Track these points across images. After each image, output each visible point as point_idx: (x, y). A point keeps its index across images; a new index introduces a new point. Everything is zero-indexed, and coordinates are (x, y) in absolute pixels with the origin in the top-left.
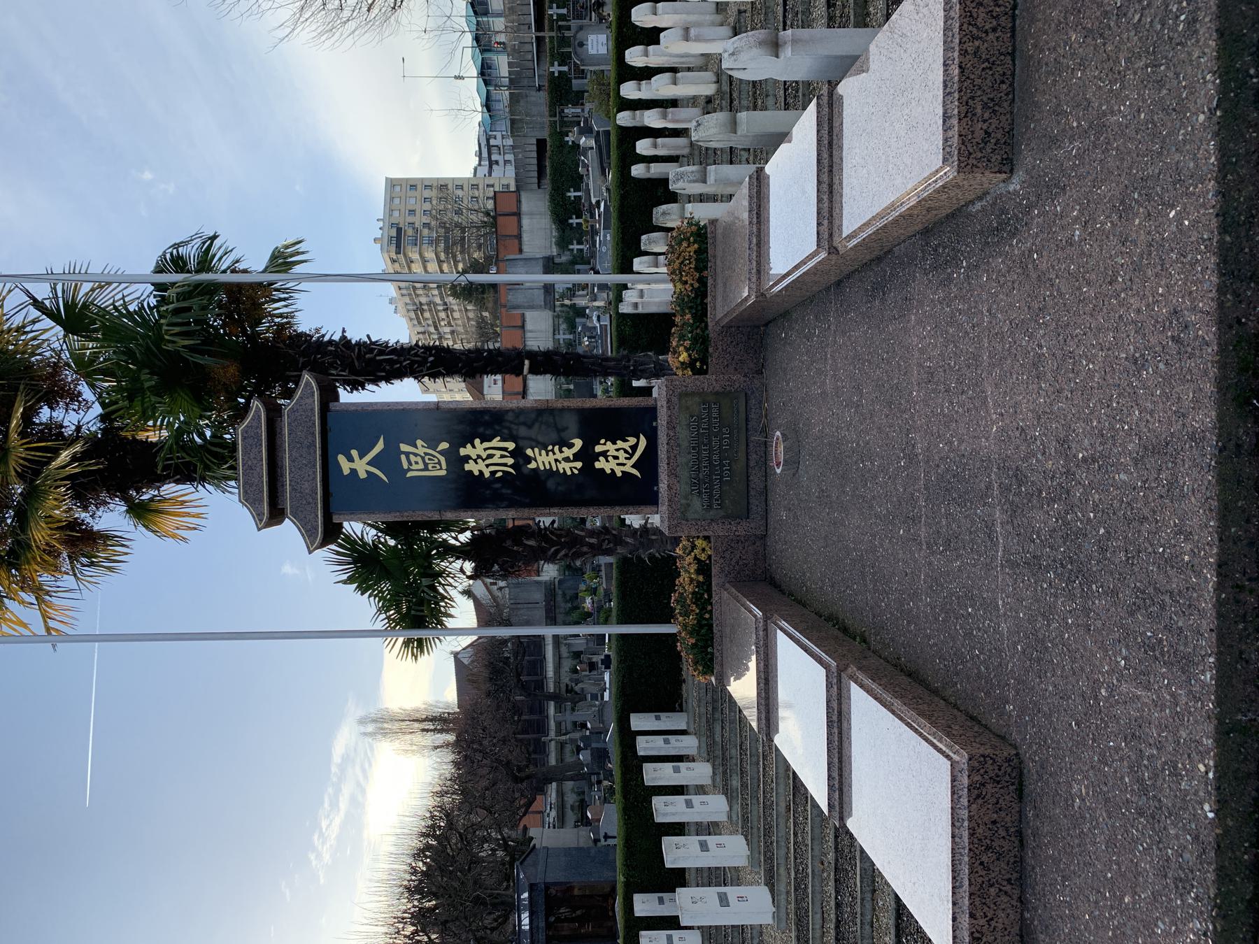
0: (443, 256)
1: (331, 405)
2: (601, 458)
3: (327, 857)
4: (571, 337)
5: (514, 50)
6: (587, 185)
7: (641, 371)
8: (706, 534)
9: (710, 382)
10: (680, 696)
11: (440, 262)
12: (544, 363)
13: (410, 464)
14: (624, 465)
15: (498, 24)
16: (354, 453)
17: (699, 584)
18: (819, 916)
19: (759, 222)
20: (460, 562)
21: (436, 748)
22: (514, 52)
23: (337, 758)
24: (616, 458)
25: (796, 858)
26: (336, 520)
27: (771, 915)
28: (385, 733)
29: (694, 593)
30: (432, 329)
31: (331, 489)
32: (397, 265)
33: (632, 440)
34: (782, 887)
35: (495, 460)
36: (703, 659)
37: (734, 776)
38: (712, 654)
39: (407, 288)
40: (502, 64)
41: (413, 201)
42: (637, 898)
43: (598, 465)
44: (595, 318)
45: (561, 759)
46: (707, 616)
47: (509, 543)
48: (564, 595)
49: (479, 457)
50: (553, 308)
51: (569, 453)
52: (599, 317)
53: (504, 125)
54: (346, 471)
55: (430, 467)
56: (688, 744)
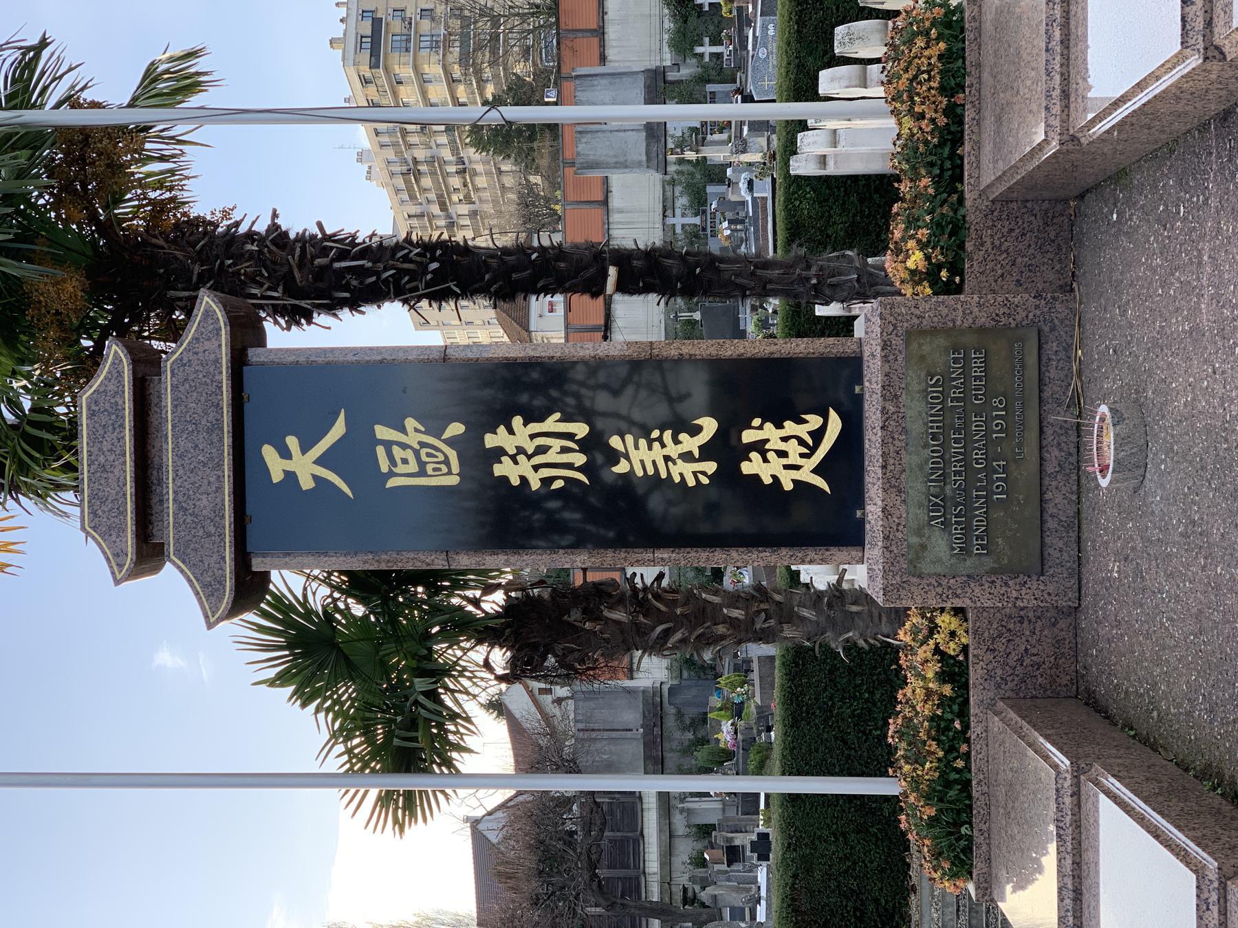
0: (457, 71)
2: (754, 455)
4: (697, 220)
7: (832, 286)
8: (958, 603)
9: (968, 308)
11: (452, 81)
14: (797, 467)
16: (292, 442)
17: (944, 702)
20: (483, 649)
24: (782, 454)
29: (932, 719)
30: (435, 209)
31: (250, 509)
32: (372, 89)
33: (814, 421)
35: (551, 457)
38: (970, 839)
43: (746, 468)
44: (743, 186)
46: (960, 764)
47: (575, 615)
48: (680, 715)
49: (521, 450)
50: (663, 167)
51: (691, 444)
52: (750, 184)
54: (277, 477)
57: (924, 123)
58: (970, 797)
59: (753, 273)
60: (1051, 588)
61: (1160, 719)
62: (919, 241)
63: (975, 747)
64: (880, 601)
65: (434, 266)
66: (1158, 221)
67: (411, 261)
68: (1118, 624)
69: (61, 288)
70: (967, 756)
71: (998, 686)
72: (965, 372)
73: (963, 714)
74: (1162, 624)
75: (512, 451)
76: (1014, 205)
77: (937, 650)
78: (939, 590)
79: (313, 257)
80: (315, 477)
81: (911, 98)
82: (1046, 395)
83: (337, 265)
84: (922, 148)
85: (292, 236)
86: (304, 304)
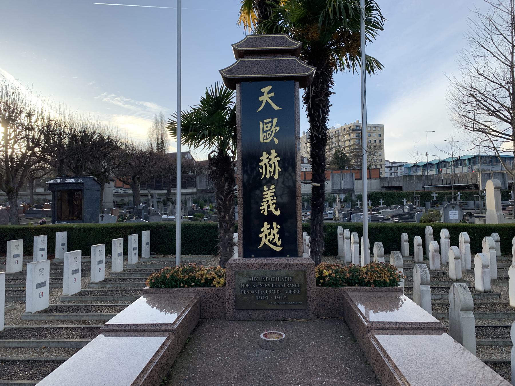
0: (352, 147)
1: (297, 84)
2: (269, 226)
3: (105, 100)
5: (439, 177)
6: (387, 209)
7: (315, 244)
8: (227, 285)
9: (312, 289)
10: (158, 254)
11: (349, 146)
12: (318, 193)
13: (267, 123)
14: (266, 238)
15: (449, 171)
16: (272, 94)
17: (200, 280)
18: (16, 345)
19: (413, 329)
20: (217, 150)
21: (151, 144)
22: (439, 178)
23: (145, 104)
24: (270, 234)
25: (54, 328)
26: (238, 86)
27: (30, 311)
28: (157, 123)
29: (195, 277)
31: (254, 83)
32: (348, 129)
34: (44, 317)
35: (268, 168)
36: (158, 282)
37: (111, 286)
38: (161, 287)
39: (338, 133)
40: (433, 172)
41: (374, 135)
42: (65, 234)
43: (266, 224)
44: (330, 212)
45: (142, 195)
46: (182, 285)
48: (212, 197)
49: (270, 160)
50: (333, 193)
51: (272, 208)
52: (331, 213)
53: (407, 173)
54: (263, 90)
55: (265, 134)
56: (133, 258)
57: (365, 275)
58: (172, 287)
59: (318, 222)
60: (231, 312)
61: (189, 354)
62: (331, 274)
63: (186, 289)
64: (228, 263)
65: (320, 137)
66: (343, 357)
67: (321, 130)
68: (220, 336)
69: (315, 33)
70: (184, 287)
71: (204, 296)
72: (294, 288)
73: (196, 285)
74: (218, 356)
75: (270, 157)
76: (342, 301)
77: (214, 278)
78: (231, 280)
79: (323, 103)
80: (263, 101)
81: (372, 271)
82: (287, 311)
83: (321, 110)
84: (357, 274)
85: (328, 98)
86: (310, 101)
